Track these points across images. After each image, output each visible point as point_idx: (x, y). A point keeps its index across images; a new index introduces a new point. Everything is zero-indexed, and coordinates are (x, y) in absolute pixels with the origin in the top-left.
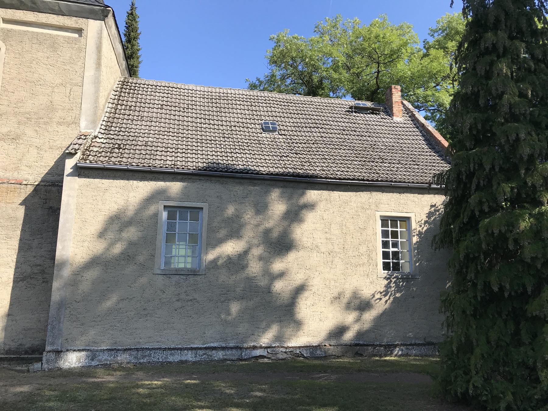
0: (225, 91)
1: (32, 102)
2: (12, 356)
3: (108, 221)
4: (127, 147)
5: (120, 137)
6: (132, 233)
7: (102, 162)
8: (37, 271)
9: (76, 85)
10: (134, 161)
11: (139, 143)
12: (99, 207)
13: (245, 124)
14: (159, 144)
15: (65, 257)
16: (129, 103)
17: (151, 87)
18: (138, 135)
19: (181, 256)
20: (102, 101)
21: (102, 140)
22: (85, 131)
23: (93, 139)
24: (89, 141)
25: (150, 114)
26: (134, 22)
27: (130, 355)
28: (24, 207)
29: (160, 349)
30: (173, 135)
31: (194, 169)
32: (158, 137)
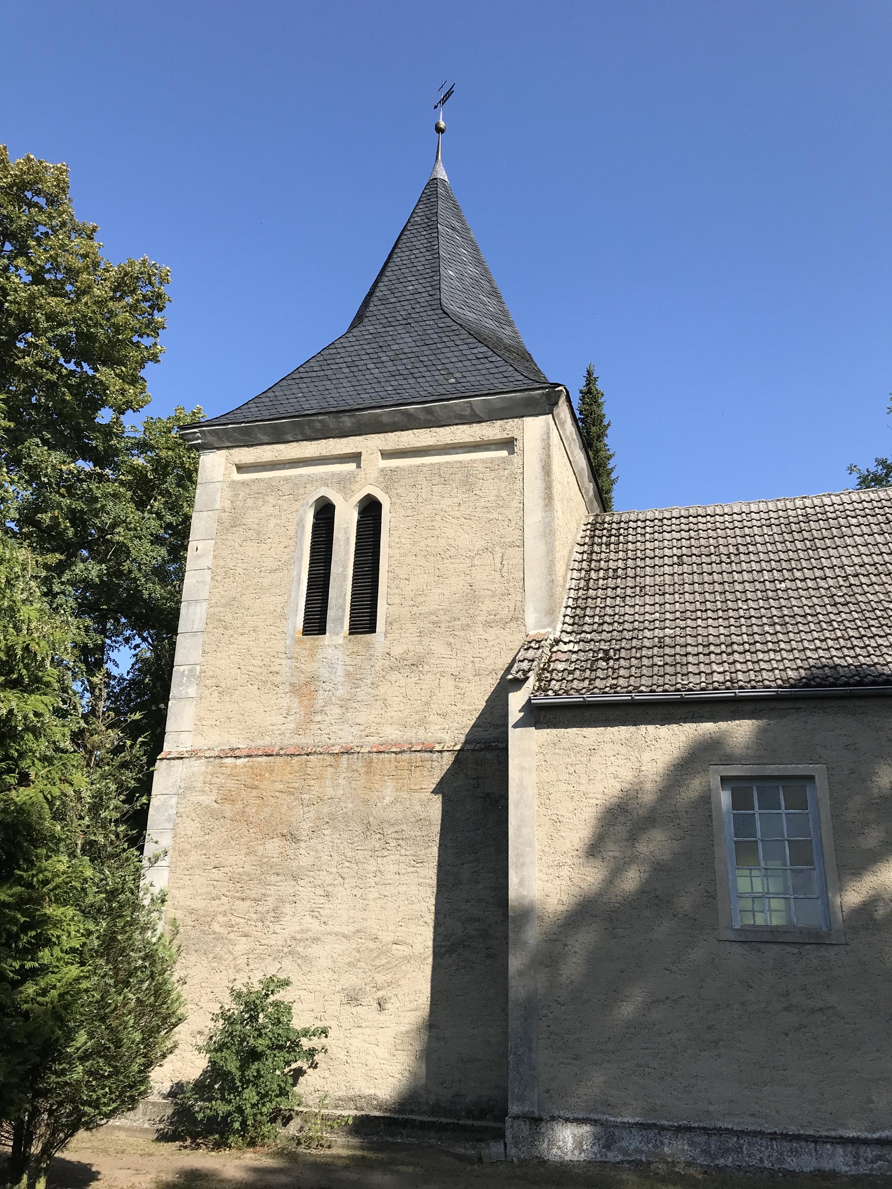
0: (817, 502)
1: (440, 591)
2: (445, 1120)
3: (605, 818)
4: (623, 653)
5: (605, 636)
6: (656, 844)
7: (578, 691)
8: (474, 933)
9: (512, 545)
10: (645, 685)
11: (647, 643)
12: (582, 788)
13: (880, 568)
14: (689, 640)
15: (526, 902)
16: (612, 565)
17: (652, 524)
18: (641, 626)
19: (759, 896)
20: (560, 568)
21: (570, 647)
22: (535, 632)
23: (552, 646)
24: (547, 650)
25: (658, 580)
26: (594, 407)
27: (692, 1144)
28: (440, 796)
29: (761, 1134)
30: (714, 616)
31: (780, 687)
32: (682, 624)
